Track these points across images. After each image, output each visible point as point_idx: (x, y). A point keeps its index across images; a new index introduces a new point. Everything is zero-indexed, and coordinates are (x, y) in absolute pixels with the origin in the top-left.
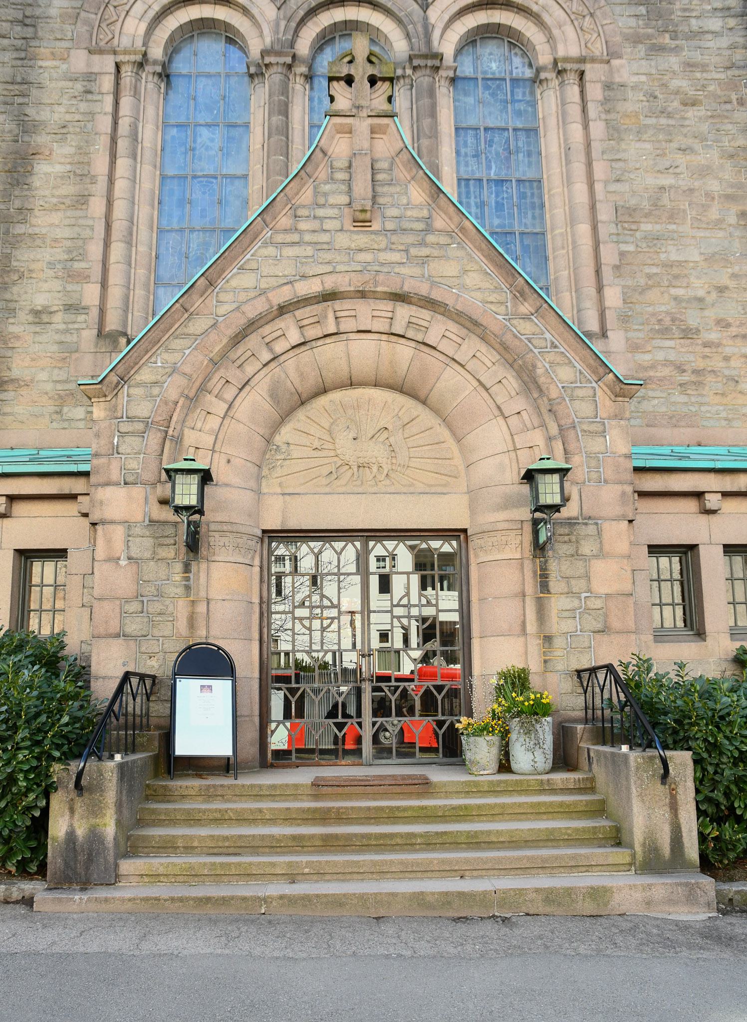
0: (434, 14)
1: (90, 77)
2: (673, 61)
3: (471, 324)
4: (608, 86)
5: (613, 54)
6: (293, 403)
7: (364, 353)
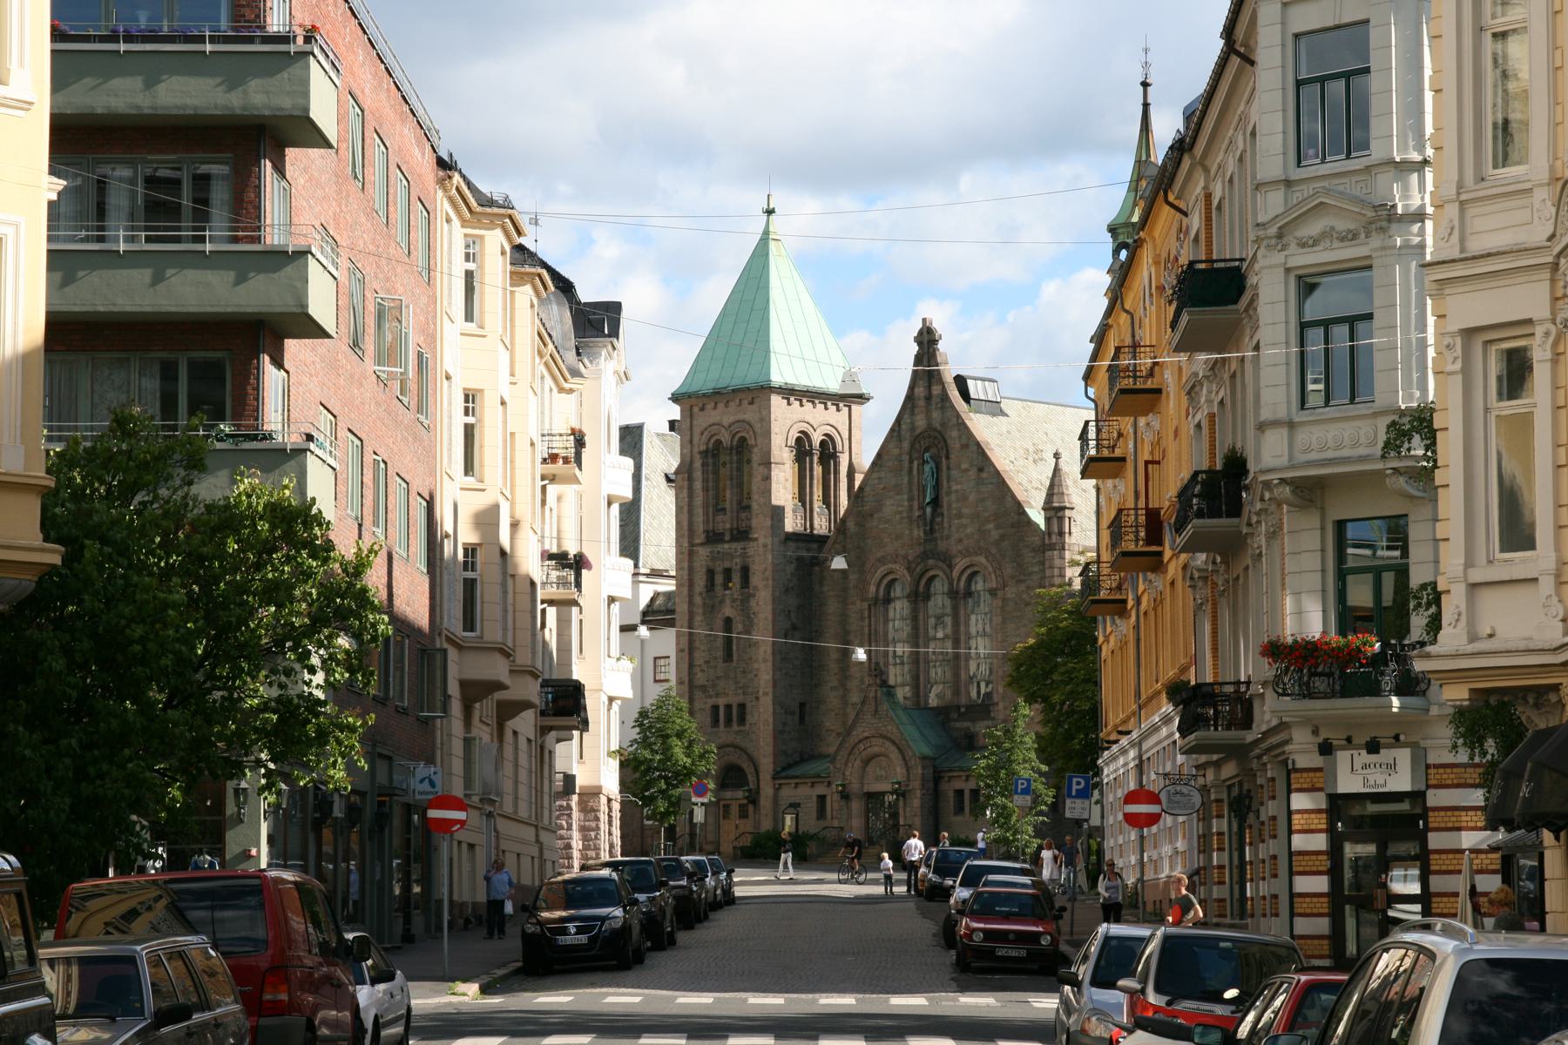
0: (955, 574)
1: (861, 611)
2: (1022, 587)
3: (894, 743)
4: (1004, 600)
5: (1005, 586)
6: (867, 762)
7: (876, 749)
